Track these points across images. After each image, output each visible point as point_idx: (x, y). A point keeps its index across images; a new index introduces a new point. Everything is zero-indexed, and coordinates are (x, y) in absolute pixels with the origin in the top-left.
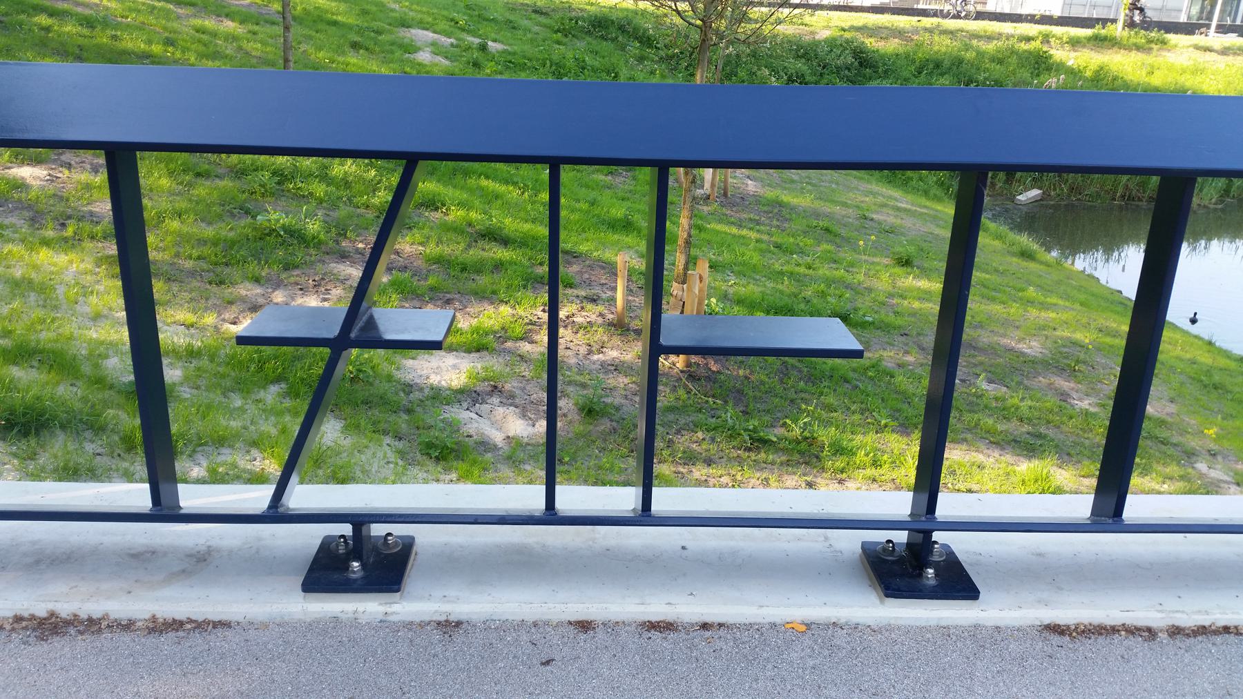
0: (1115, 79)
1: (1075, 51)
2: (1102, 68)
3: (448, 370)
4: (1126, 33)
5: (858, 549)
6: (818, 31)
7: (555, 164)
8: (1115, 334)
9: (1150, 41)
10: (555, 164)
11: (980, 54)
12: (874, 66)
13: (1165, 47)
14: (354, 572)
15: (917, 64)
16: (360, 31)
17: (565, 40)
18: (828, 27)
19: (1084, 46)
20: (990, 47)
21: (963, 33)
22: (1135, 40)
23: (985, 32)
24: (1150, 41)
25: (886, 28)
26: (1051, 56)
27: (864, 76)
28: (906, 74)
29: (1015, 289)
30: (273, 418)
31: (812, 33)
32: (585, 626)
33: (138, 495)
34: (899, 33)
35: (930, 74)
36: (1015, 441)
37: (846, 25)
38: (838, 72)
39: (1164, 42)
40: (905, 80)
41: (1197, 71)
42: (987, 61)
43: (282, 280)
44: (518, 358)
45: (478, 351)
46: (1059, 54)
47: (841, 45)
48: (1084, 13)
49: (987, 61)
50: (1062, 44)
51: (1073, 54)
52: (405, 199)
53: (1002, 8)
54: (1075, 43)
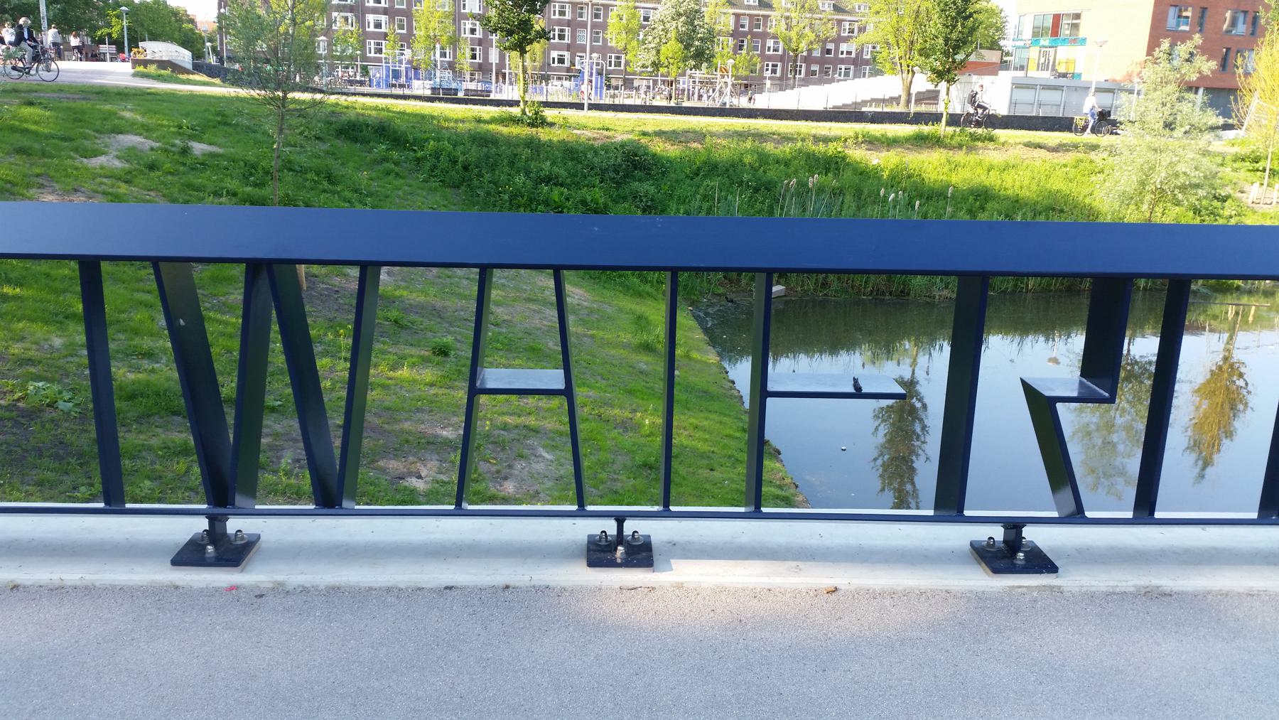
7: (557, 271)
12: (649, 169)
14: (209, 553)
18: (628, 132)
20: (786, 149)
21: (775, 137)
24: (974, 138)
30: (182, 460)
32: (15, 587)
34: (700, 136)
35: (705, 176)
37: (649, 129)
39: (991, 139)
46: (857, 154)
48: (1032, 111)
52: (1130, 316)
53: (954, 109)
54: (873, 143)
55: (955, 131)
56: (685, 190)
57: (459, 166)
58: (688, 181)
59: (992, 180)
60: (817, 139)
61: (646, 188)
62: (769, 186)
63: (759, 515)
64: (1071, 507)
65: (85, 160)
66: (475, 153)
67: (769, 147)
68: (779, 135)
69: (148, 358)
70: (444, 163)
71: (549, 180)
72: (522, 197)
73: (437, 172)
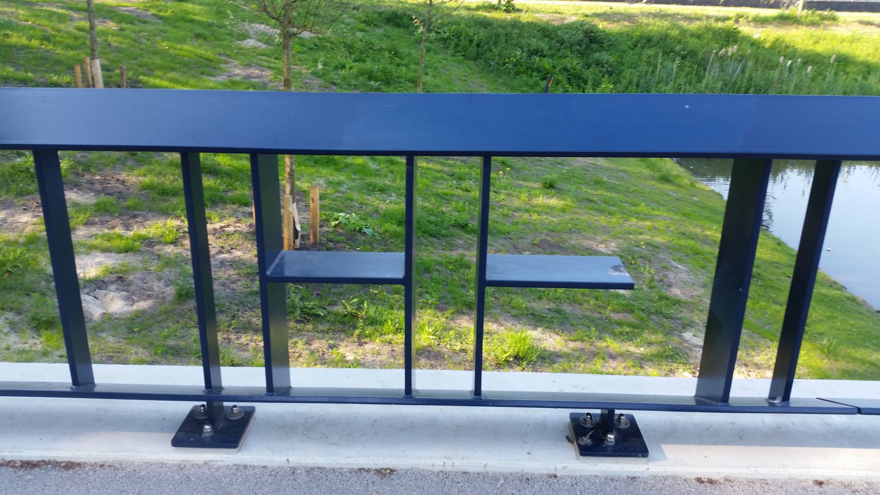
0: (787, 47)
1: (763, 27)
2: (777, 40)
3: (92, 266)
4: (805, 12)
5: (568, 420)
6: (566, 17)
7: (411, 156)
8: (705, 240)
9: (823, 18)
10: (411, 156)
11: (683, 32)
12: (601, 43)
13: (835, 22)
15: (634, 40)
16: (209, 25)
17: (367, 28)
18: (576, 14)
19: (771, 24)
20: (694, 26)
21: (679, 16)
22: (812, 18)
23: (696, 15)
24: (823, 18)
25: (620, 14)
26: (739, 32)
27: (592, 50)
28: (624, 47)
29: (630, 204)
31: (563, 19)
33: (394, 380)
34: (629, 17)
35: (643, 47)
36: (532, 314)
37: (589, 12)
38: (571, 47)
39: (834, 19)
40: (623, 51)
41: (853, 40)
42: (688, 36)
43: (14, 204)
44: (156, 257)
45: (127, 251)
46: (746, 30)
47: (577, 27)
49: (688, 36)
50: (749, 22)
51: (755, 30)
55: (807, 13)
56: (630, 57)
57: (474, 44)
58: (631, 52)
59: (845, 49)
60: (718, 19)
61: (604, 56)
62: (692, 53)
63: (728, 409)
64: (720, 393)
65: (240, 42)
66: (482, 33)
67: (684, 24)
68: (682, 15)
69: (9, 241)
70: (464, 43)
71: (536, 52)
72: (521, 66)
73: (459, 48)
